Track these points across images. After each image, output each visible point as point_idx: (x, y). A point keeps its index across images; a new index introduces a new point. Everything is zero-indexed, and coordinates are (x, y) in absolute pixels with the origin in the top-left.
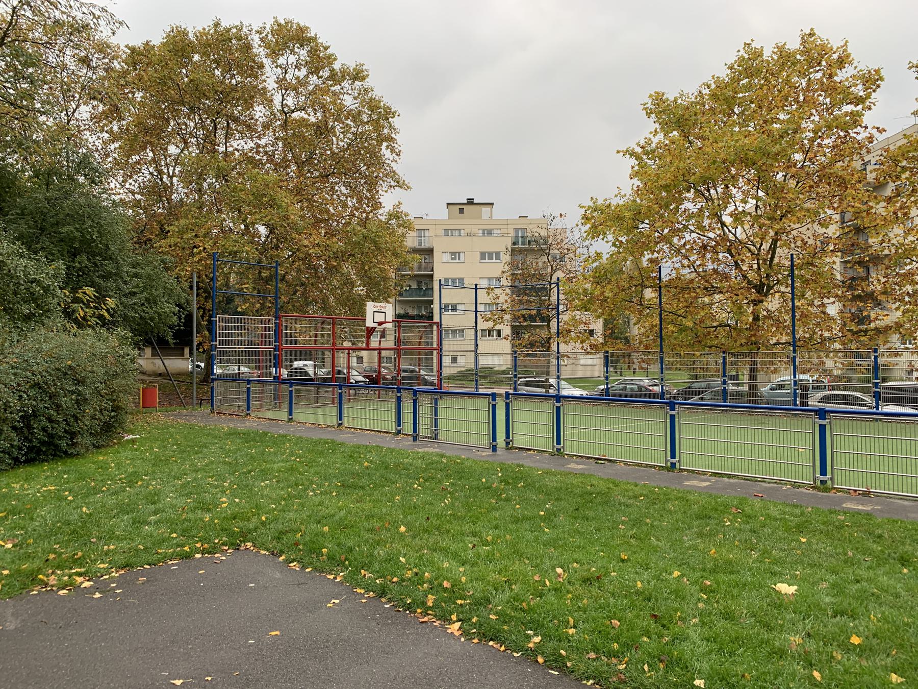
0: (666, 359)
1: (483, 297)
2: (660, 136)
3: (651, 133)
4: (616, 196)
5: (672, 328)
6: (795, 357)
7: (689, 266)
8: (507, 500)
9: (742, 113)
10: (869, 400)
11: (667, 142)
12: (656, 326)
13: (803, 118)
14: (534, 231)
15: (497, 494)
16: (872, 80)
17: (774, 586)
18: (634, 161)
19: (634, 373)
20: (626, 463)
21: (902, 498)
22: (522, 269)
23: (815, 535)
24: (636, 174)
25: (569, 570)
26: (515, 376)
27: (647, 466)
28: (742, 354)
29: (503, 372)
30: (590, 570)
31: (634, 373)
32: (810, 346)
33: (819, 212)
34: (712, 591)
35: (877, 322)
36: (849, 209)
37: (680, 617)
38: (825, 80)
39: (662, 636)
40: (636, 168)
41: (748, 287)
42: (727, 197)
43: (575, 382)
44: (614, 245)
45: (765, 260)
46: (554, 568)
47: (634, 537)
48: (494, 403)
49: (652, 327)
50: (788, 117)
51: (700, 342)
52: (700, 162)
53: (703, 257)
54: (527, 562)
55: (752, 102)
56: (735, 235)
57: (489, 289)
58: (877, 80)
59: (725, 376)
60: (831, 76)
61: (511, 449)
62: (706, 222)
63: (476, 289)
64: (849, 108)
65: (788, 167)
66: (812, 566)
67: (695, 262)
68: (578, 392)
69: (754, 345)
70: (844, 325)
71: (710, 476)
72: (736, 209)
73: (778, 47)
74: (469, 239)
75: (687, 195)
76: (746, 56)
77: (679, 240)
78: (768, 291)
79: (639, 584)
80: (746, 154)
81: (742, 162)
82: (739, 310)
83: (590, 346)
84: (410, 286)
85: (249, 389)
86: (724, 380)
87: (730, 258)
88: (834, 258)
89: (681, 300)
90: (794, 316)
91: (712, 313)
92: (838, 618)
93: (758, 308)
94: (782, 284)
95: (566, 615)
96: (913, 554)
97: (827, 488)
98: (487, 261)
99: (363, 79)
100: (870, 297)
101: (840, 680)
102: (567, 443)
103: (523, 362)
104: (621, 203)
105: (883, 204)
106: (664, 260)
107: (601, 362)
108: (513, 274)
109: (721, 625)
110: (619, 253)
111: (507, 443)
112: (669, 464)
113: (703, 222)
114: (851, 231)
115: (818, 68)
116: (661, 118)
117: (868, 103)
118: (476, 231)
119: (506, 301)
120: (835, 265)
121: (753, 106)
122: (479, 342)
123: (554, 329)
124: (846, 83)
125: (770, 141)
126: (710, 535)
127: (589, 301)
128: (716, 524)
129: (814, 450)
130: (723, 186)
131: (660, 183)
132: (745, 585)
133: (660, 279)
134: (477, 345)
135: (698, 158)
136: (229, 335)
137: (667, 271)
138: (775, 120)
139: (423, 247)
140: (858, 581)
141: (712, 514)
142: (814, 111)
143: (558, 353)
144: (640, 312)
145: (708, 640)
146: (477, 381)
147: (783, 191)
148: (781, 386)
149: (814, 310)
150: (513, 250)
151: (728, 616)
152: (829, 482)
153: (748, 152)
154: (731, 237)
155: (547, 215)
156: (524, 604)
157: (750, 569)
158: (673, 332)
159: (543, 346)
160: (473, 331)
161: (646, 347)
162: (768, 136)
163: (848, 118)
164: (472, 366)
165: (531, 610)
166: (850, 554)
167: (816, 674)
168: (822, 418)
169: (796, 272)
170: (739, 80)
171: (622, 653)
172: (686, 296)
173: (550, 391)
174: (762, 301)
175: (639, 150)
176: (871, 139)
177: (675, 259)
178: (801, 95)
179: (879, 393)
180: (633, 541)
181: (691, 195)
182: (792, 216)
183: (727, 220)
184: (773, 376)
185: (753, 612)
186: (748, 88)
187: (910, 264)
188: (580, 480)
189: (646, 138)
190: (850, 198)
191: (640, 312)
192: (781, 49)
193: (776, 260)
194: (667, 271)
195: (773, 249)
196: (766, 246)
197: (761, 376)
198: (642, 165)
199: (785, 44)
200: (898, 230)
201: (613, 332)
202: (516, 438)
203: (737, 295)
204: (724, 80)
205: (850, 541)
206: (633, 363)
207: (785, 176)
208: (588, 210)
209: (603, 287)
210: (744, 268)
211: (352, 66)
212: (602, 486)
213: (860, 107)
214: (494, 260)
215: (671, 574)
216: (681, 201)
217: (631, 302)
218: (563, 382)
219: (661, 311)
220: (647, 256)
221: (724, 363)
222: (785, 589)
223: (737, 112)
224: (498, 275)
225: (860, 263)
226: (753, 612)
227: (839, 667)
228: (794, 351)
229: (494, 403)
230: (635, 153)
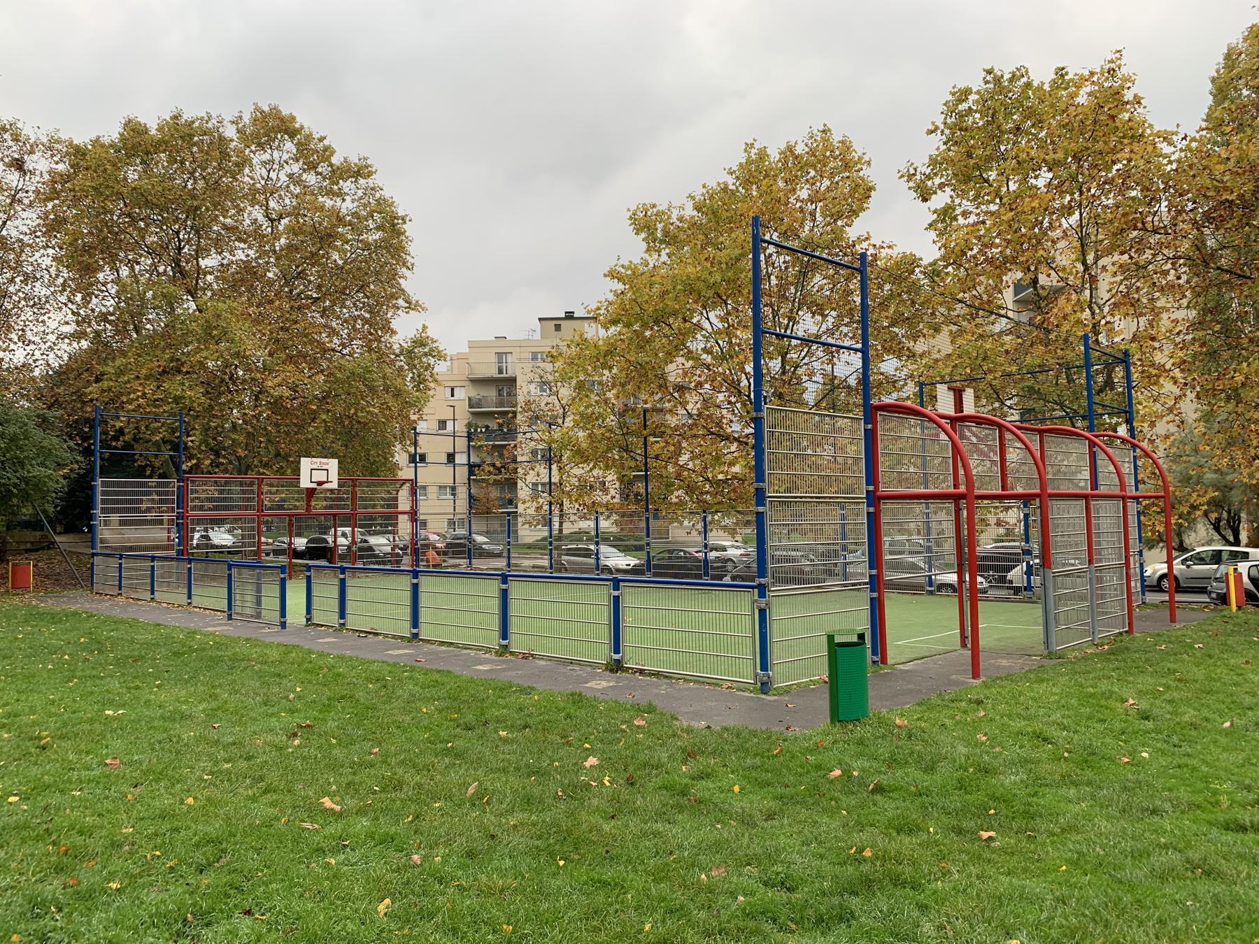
84: (487, 427)
99: (370, 174)
111: (308, 620)
136: (244, 492)
139: (504, 375)
211: (354, 159)
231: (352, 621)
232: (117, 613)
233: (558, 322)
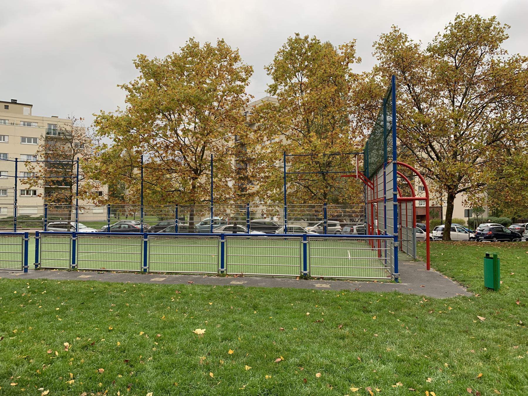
0: (144, 209)
1: (21, 167)
2: (143, 80)
3: (138, 78)
4: (117, 111)
5: (148, 192)
6: (212, 208)
7: (159, 157)
8: (33, 303)
9: (188, 75)
10: (245, 229)
11: (148, 85)
12: (139, 190)
13: (218, 84)
14: (61, 126)
15: (25, 300)
16: (249, 71)
17: (194, 331)
18: (127, 93)
19: (127, 217)
20: (117, 272)
21: (256, 276)
22: (53, 151)
23: (216, 300)
24: (129, 100)
25: (73, 342)
26: (46, 221)
27: (130, 272)
28: (186, 206)
29: (37, 218)
30: (87, 340)
31: (127, 217)
32: (219, 202)
33: (224, 134)
34: (161, 340)
35: (249, 190)
36: (238, 134)
37: (141, 358)
38: (228, 67)
39: (130, 372)
40: (129, 97)
41: (190, 170)
42: (180, 120)
43: (88, 224)
44: (115, 140)
45: (199, 156)
46: (62, 343)
47: (118, 316)
48: (27, 239)
49: (137, 190)
50: (211, 82)
51: (164, 199)
52: (165, 99)
53: (166, 152)
54: (43, 342)
55: (193, 71)
56: (184, 142)
57: (27, 162)
58: (251, 71)
59: (177, 218)
60: (231, 65)
61: (39, 269)
62: (169, 133)
63: (16, 161)
64: (238, 83)
65: (211, 109)
66: (214, 317)
67: (162, 155)
68: (90, 230)
69: (193, 201)
70: (235, 192)
71: (166, 274)
72: (185, 127)
73: (207, 44)
74: (12, 127)
75: (159, 116)
76: (191, 45)
77: (153, 141)
78: (200, 172)
79: (119, 343)
80: (190, 98)
81: (188, 102)
82: (185, 182)
83: (99, 201)
86: (177, 220)
87: (181, 153)
88: (231, 158)
89: (154, 175)
90: (212, 186)
91: (171, 184)
92: (224, 342)
93: (195, 181)
94: (206, 170)
95: (68, 372)
96: (259, 303)
97: (224, 275)
98: (26, 143)
100: (246, 178)
101: (222, 375)
102: (80, 262)
103: (52, 211)
104: (120, 116)
105: (253, 133)
106: (145, 152)
107: (106, 211)
108: (46, 154)
109: (164, 358)
110: (118, 145)
111: (36, 266)
112: (143, 270)
113: (166, 132)
114: (239, 145)
115: (225, 60)
116: (144, 70)
117: (247, 82)
118: (19, 122)
119: (40, 171)
120: (232, 162)
121: (194, 73)
122: (18, 198)
123: (74, 191)
124: (238, 70)
125: (201, 93)
126: (163, 308)
127: (98, 173)
128: (167, 301)
129: (218, 255)
130: (177, 114)
131: (142, 107)
132: (179, 333)
133: (142, 163)
134: (16, 200)
135: (164, 96)
137: (147, 158)
138: (205, 83)
140: (234, 321)
141: (165, 296)
142: (223, 81)
143: (77, 205)
144: (130, 182)
145: (157, 368)
146: (15, 225)
147: (207, 121)
148: (206, 223)
149: (221, 183)
150: (46, 137)
151: (169, 352)
152: (225, 272)
153: (191, 97)
154: (182, 142)
155: (71, 117)
156: (38, 371)
157: (183, 324)
158: (149, 193)
159: (66, 201)
160: (13, 191)
161: (133, 202)
162: (201, 90)
163: (238, 88)
164: (12, 214)
165: (43, 373)
166: (232, 307)
167: (211, 374)
168: (223, 239)
169: (214, 164)
170: (187, 57)
171: (104, 388)
172: (157, 173)
173: (71, 230)
174: (197, 178)
175: (131, 87)
176: (248, 100)
177: (151, 152)
178: (217, 72)
179: (249, 225)
180: (117, 318)
181: (160, 116)
182: (212, 134)
183: (180, 133)
184: (202, 218)
185: (182, 347)
186: (191, 62)
187: (263, 163)
188: (86, 285)
189: (135, 80)
190: (239, 129)
191: (130, 182)
192: (208, 46)
193: (204, 157)
194: (147, 158)
195: (203, 151)
196: (199, 149)
197: (196, 218)
198: (133, 96)
199: (210, 43)
200: (259, 147)
201: (114, 193)
202: (43, 262)
203: (184, 174)
204: (179, 55)
205: (232, 301)
206: (125, 211)
207: (209, 113)
208: (99, 117)
209: (107, 165)
210: (189, 160)
212: (101, 287)
213: (243, 83)
214: (26, 143)
215: (139, 334)
216: (155, 119)
217: (125, 175)
218: (80, 224)
219: (142, 182)
220: (135, 149)
221: (177, 211)
222: (200, 331)
223: (186, 75)
224: (34, 153)
225: (243, 161)
226: (182, 347)
227: (222, 367)
228: (212, 205)
229: (27, 239)
230: (128, 88)
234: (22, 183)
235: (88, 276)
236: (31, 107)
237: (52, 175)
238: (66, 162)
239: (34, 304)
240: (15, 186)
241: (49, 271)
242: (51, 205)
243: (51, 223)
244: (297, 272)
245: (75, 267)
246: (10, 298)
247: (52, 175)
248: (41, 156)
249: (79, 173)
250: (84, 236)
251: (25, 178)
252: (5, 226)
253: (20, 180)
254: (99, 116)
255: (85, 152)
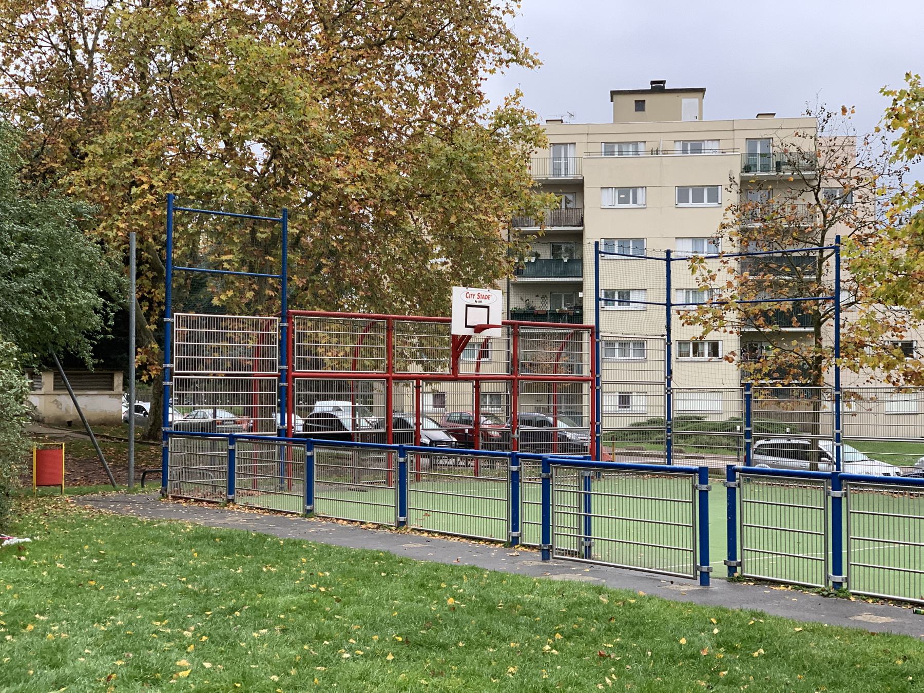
1: (682, 276)
29: (724, 426)
48: (704, 487)
57: (695, 261)
61: (740, 579)
63: (668, 260)
68: (878, 469)
74: (655, 161)
83: (905, 375)
84: (537, 255)
85: (232, 452)
102: (855, 571)
103: (765, 405)
108: (744, 231)
111: (732, 569)
118: (670, 146)
119: (730, 284)
122: (674, 366)
123: (828, 341)
127: (902, 284)
134: (670, 372)
139: (563, 178)
143: (838, 388)
146: (669, 443)
150: (744, 182)
155: (815, 110)
159: (805, 374)
160: (662, 345)
164: (660, 413)
173: (821, 466)
202: (749, 558)
208: (900, 98)
218: (847, 449)
224: (712, 232)
229: (704, 487)
231: (415, 519)
232: (807, 615)
233: (640, 97)
234: (683, 321)
235: (884, 619)
236: (701, 94)
237: (762, 294)
238: (802, 253)
239: (736, 685)
240: (665, 333)
241: (766, 590)
242: (762, 385)
243: (762, 442)
244: (819, 577)
245: (841, 584)
246: (673, 659)
247: (762, 295)
248: (731, 239)
249: (841, 284)
250: (861, 486)
251: (688, 307)
252: (643, 446)
253: (678, 312)
254: (902, 93)
255: (860, 215)
